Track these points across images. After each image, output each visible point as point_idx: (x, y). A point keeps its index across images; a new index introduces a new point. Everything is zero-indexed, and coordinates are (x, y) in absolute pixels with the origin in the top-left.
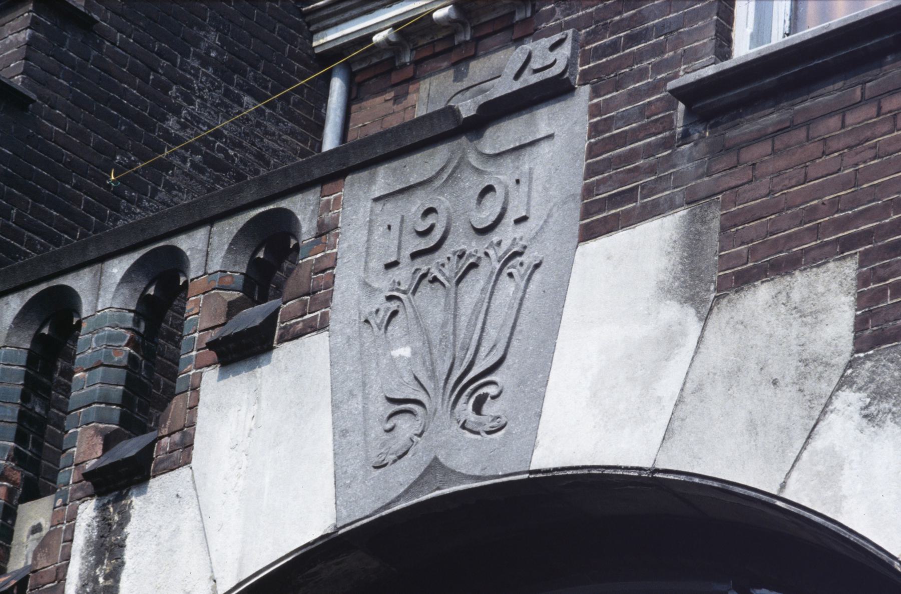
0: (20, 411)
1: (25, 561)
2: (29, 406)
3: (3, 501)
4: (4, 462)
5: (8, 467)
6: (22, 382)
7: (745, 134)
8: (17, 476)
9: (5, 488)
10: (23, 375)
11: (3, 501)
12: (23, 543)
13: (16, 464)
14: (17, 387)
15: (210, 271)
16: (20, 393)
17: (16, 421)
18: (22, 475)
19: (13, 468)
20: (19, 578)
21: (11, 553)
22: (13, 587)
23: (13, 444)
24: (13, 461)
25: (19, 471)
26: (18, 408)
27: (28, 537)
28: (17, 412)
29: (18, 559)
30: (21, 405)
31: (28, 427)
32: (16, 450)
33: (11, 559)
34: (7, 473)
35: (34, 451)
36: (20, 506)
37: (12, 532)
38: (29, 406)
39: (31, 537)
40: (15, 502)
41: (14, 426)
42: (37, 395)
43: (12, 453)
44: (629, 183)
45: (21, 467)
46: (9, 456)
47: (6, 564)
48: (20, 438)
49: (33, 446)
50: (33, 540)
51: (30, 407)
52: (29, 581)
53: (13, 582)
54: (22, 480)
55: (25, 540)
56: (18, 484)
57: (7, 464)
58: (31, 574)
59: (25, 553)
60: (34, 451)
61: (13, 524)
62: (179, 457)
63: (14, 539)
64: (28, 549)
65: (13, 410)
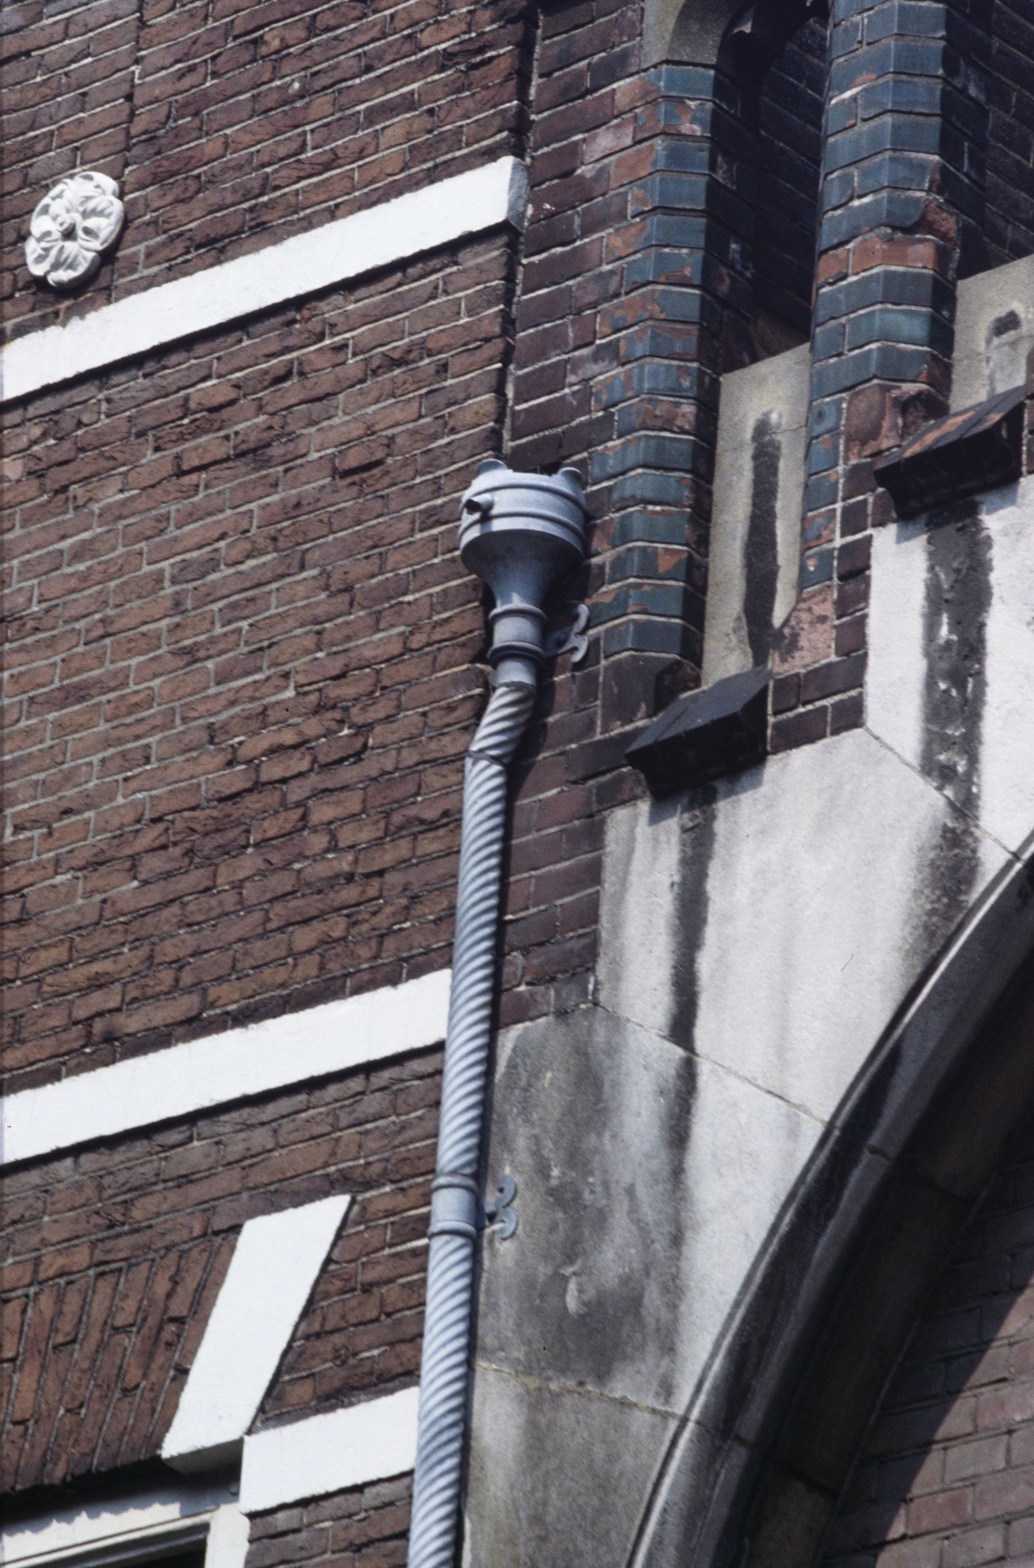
0: (944, 92)
1: (988, 388)
2: (958, 82)
3: (931, 272)
4: (923, 194)
5: (933, 205)
6: (942, 33)
7: (949, 433)
8: (949, 223)
9: (932, 245)
10: (942, 19)
11: (931, 272)
12: (979, 354)
13: (947, 201)
14: (932, 43)
15: (42, 1276)
16: (939, 57)
17: (939, 112)
18: (957, 222)
19: (939, 207)
20: (1009, 406)
21: (954, 376)
22: (998, 425)
23: (936, 158)
24: (940, 192)
25: (951, 214)
26: (940, 86)
27: (988, 342)
28: (938, 93)
29: (971, 386)
30: (944, 79)
31: (959, 125)
32: (944, 171)
33: (955, 388)
34: (931, 217)
35: (973, 174)
36: (960, 283)
37: (951, 333)
38: (958, 82)
39: (996, 341)
40: (951, 274)
41: (936, 121)
42: (970, 63)
43: (938, 177)
44: (605, 617)
45: (955, 206)
46: (932, 182)
47: (947, 397)
48: (947, 147)
49: (971, 164)
50: (1001, 346)
51: (959, 86)
52: (1026, 416)
53: (995, 417)
54: (959, 230)
55: (982, 347)
56: (950, 240)
57: (931, 198)
58: (1028, 402)
59: (987, 372)
60: (973, 174)
61: (952, 319)
62: (230, 847)
63: (956, 346)
64: (991, 364)
65: (931, 91)
